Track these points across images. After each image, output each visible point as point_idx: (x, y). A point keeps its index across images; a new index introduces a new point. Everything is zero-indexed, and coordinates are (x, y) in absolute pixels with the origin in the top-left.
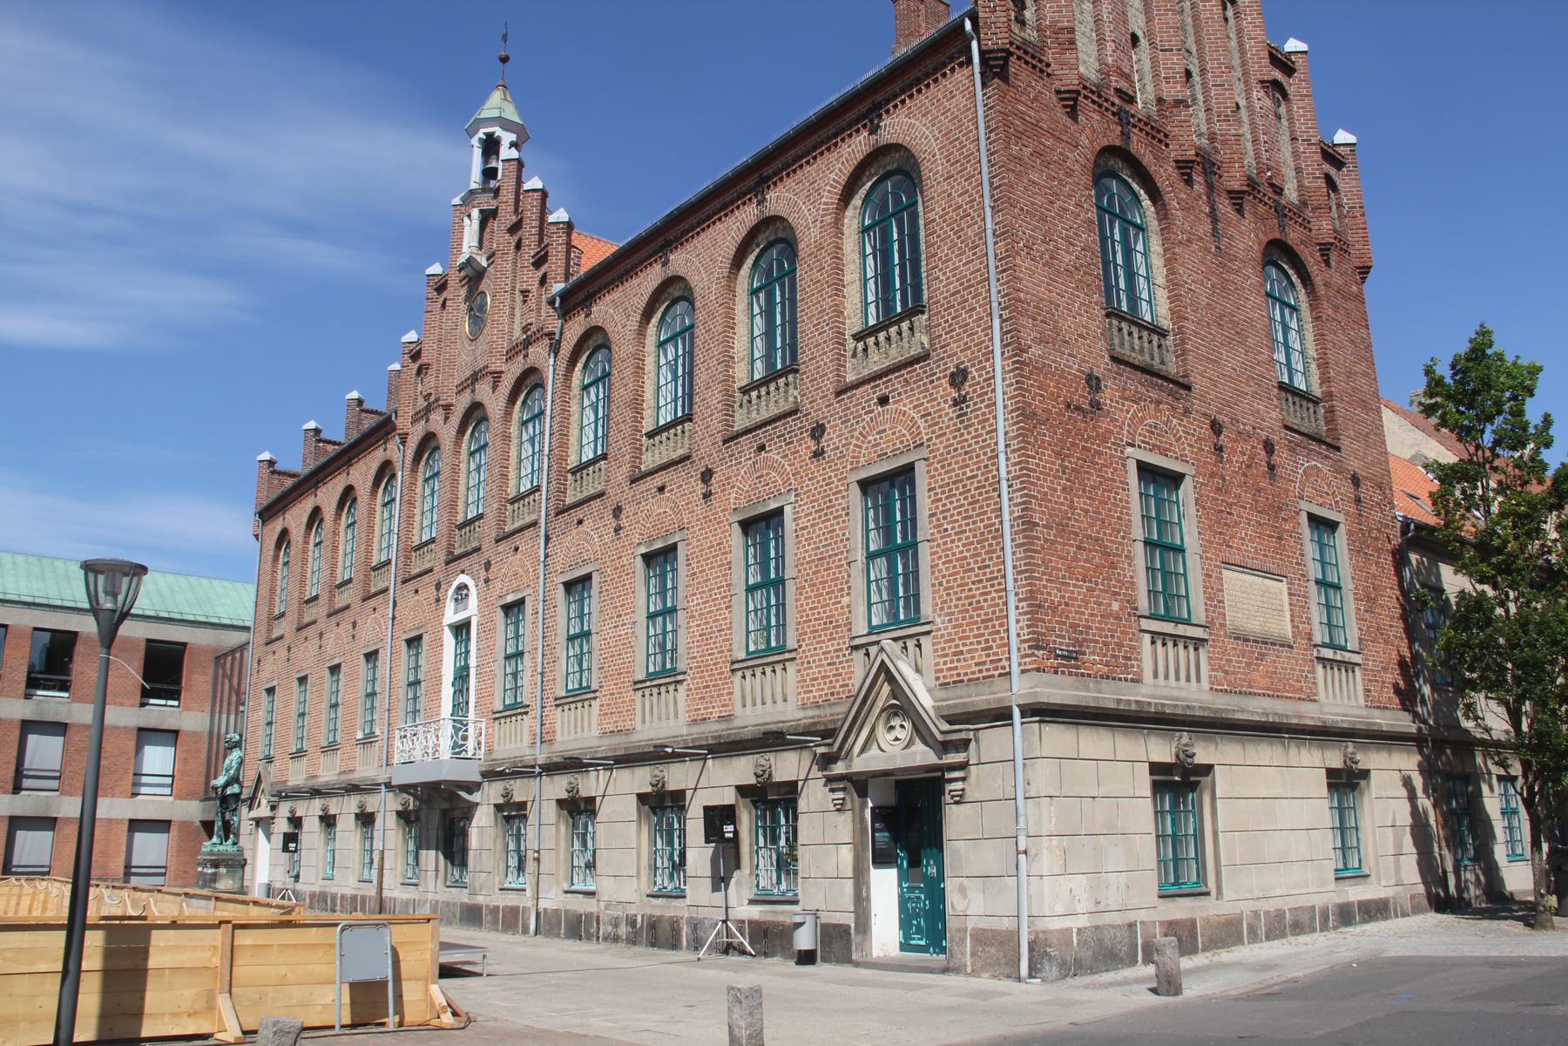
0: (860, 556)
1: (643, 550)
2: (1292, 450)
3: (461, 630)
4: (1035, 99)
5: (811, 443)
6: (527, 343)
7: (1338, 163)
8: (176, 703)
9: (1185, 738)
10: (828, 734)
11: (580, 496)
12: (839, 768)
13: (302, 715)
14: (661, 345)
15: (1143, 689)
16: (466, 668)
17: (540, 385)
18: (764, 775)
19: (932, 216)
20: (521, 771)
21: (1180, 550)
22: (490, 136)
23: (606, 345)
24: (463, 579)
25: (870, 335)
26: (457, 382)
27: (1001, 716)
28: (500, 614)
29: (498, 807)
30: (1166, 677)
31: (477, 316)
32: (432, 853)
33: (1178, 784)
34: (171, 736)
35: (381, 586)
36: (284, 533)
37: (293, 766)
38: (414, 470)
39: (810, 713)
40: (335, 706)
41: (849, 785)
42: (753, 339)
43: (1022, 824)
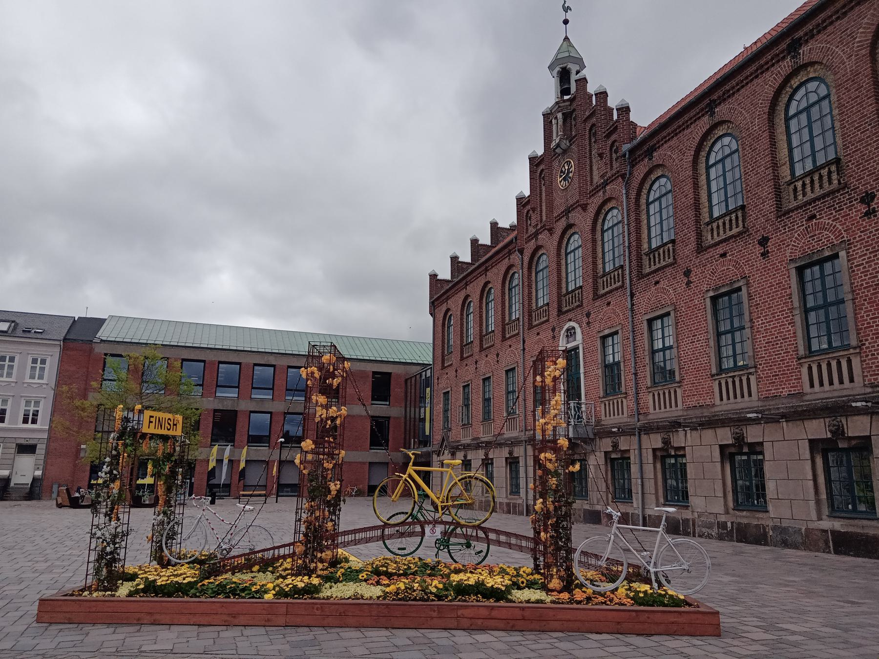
1: (711, 294)
24: (572, 324)
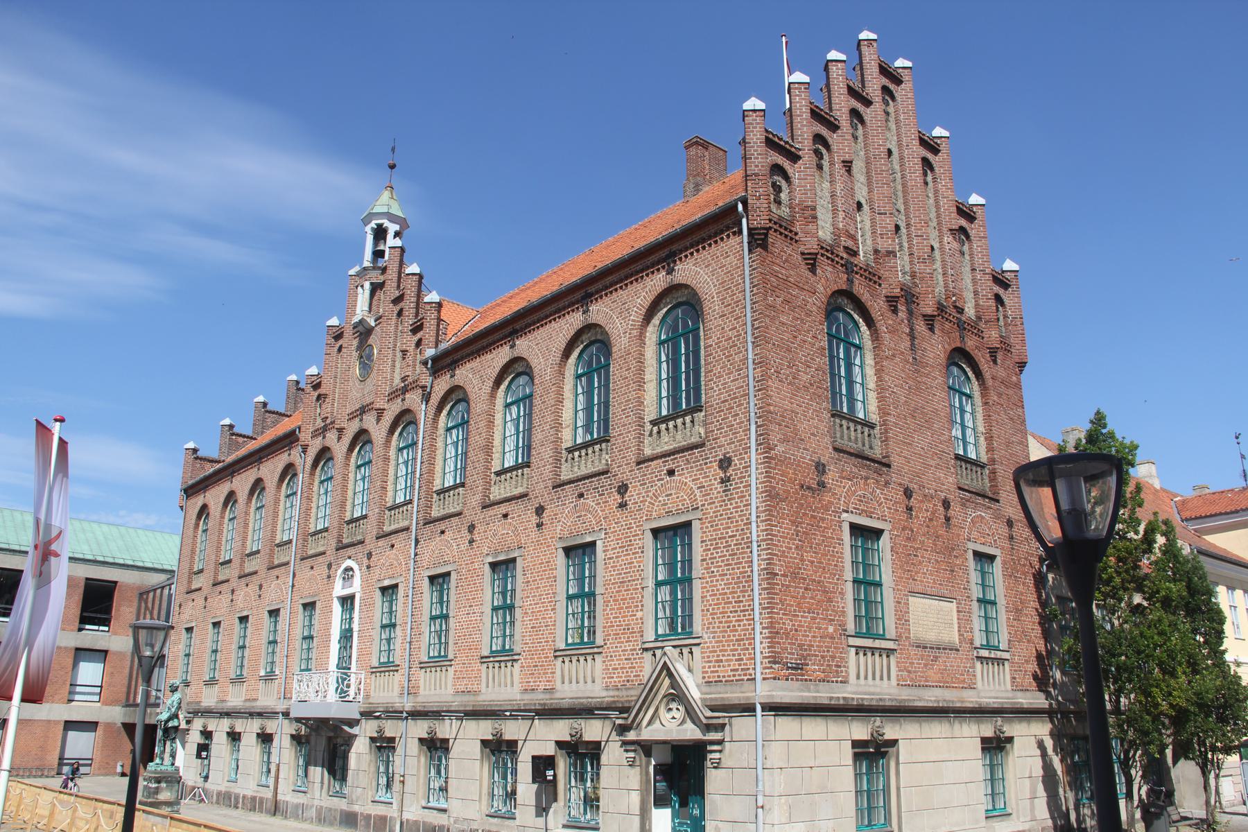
0: (650, 583)
1: (490, 559)
2: (963, 505)
3: (347, 601)
4: (786, 261)
5: (618, 497)
6: (405, 390)
7: (1005, 285)
8: (106, 629)
9: (878, 721)
10: (624, 710)
11: (442, 512)
12: (631, 736)
13: (215, 651)
14: (508, 406)
15: (849, 688)
16: (350, 630)
17: (414, 422)
18: (577, 735)
19: (710, 342)
20: (393, 714)
21: (879, 585)
22: (380, 226)
23: (465, 399)
24: (349, 563)
25: (663, 422)
26: (349, 411)
27: (749, 709)
28: (378, 593)
29: (373, 739)
30: (866, 678)
31: (366, 361)
32: (319, 769)
33: (872, 754)
34: (101, 654)
35: (285, 560)
36: (204, 508)
37: (206, 691)
38: (312, 473)
39: (611, 693)
40: (243, 647)
41: (638, 748)
42: (576, 412)
43: (760, 787)
